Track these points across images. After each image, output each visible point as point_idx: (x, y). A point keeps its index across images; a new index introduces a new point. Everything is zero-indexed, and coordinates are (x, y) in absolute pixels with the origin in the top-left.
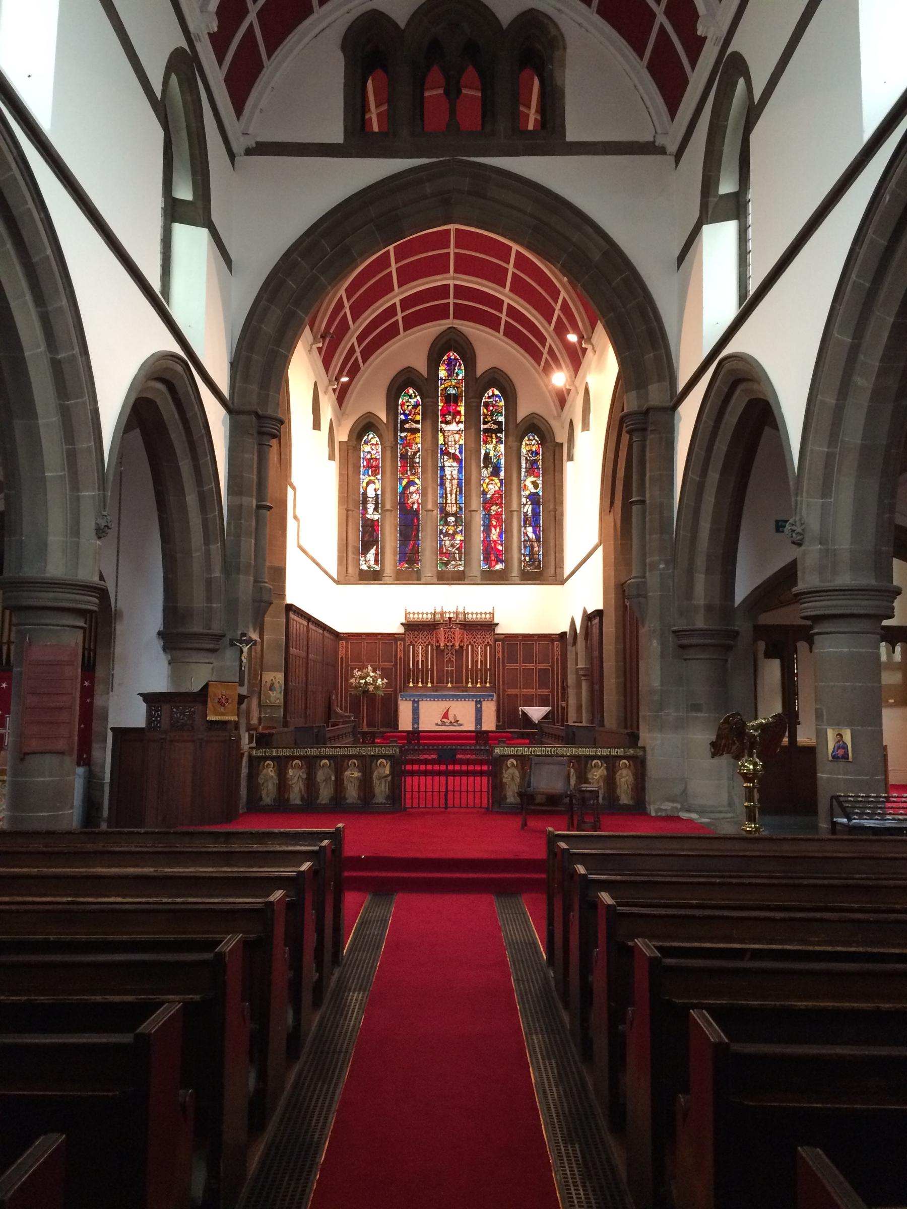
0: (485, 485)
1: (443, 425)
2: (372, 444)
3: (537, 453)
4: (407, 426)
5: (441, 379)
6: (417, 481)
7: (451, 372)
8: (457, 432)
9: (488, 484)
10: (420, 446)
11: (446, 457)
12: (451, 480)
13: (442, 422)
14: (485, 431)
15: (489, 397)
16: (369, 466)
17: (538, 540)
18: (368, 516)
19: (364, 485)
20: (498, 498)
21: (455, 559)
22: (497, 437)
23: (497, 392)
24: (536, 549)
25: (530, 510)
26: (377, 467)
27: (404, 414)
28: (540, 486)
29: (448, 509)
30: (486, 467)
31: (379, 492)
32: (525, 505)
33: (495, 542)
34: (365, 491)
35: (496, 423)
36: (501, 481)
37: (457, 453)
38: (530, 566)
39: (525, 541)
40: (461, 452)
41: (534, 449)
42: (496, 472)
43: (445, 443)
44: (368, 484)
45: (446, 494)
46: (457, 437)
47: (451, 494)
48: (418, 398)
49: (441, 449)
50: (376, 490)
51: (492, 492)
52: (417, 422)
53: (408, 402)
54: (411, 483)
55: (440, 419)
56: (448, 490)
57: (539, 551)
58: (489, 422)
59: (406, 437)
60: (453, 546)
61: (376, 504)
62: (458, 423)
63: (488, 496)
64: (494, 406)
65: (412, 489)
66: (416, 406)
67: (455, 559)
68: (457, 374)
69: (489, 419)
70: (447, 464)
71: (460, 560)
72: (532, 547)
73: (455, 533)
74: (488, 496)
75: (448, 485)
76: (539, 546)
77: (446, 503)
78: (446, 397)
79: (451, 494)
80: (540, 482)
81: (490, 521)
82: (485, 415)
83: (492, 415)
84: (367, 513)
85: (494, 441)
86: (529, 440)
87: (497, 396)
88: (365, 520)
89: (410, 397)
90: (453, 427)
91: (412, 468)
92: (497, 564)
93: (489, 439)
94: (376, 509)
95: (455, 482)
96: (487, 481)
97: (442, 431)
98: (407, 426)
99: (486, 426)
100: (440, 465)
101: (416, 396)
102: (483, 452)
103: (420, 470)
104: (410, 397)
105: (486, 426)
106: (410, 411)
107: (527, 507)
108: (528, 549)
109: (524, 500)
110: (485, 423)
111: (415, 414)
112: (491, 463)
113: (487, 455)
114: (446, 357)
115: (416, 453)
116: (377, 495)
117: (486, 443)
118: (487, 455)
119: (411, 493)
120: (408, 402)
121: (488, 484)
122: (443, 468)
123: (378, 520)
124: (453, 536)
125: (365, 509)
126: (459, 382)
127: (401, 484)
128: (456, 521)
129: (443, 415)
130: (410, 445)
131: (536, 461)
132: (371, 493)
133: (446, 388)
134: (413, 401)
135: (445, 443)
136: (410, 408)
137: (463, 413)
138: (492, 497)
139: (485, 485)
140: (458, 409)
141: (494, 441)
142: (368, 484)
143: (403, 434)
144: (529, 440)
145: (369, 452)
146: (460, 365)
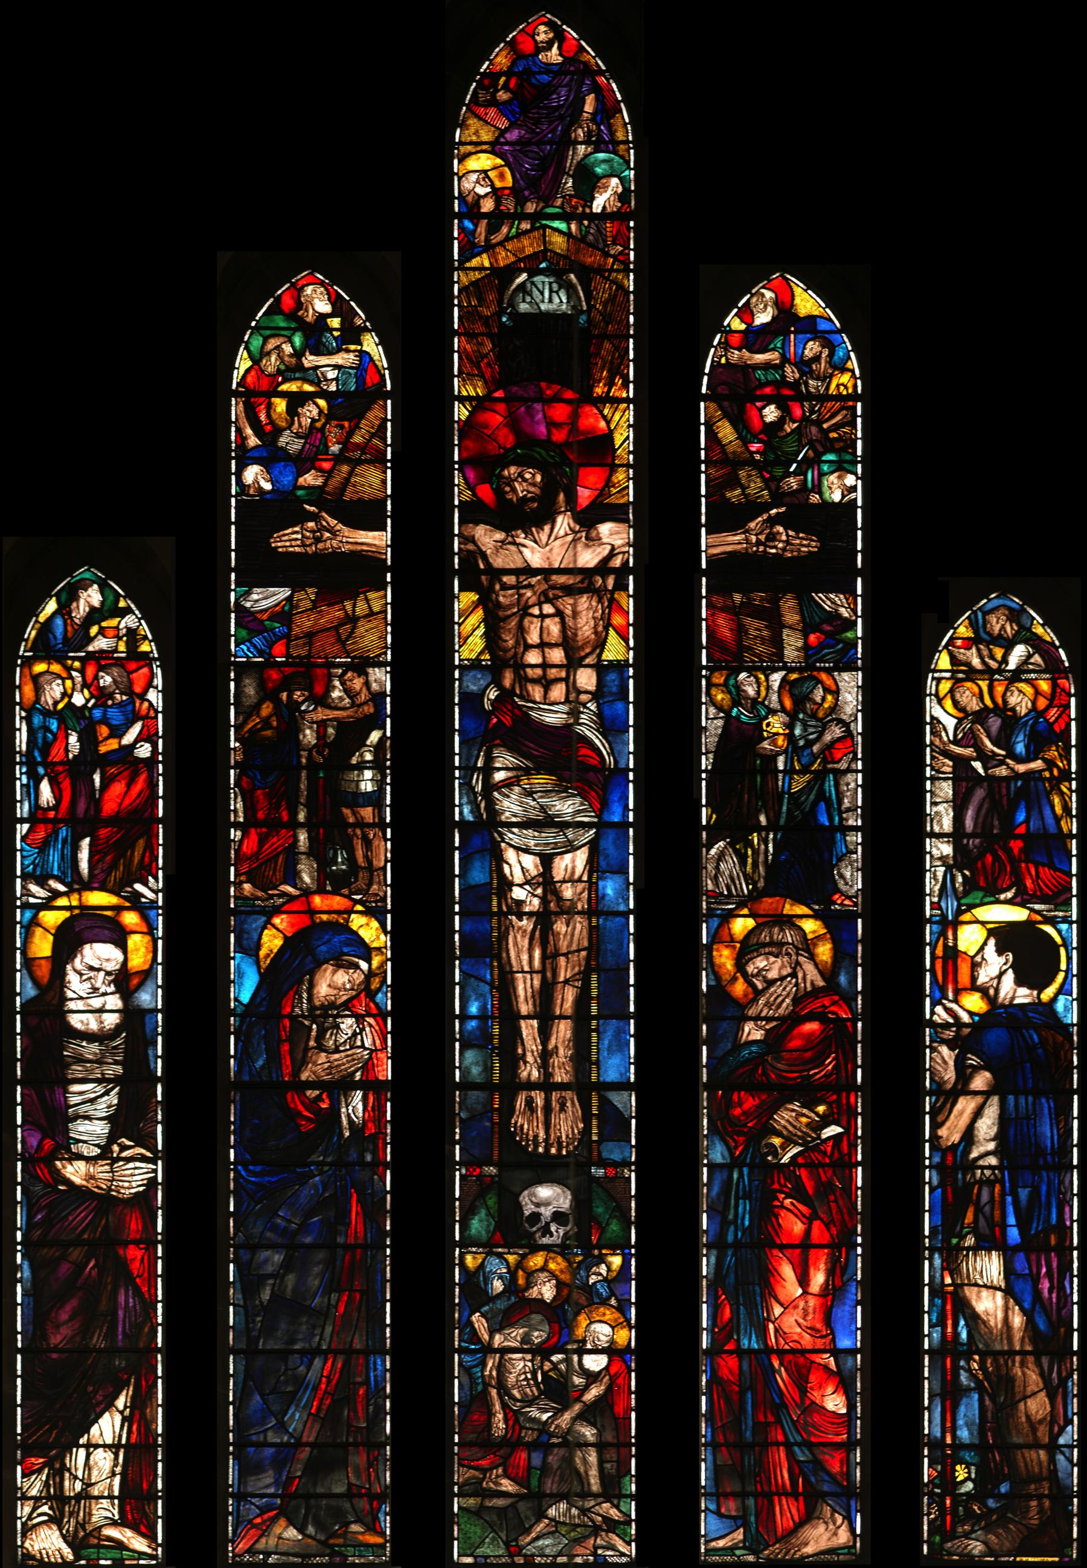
0: (725, 958)
1: (487, 537)
2: (103, 660)
3: (1043, 735)
4: (289, 540)
5: (472, 209)
6: (368, 929)
7: (540, 171)
8: (585, 581)
9: (747, 948)
10: (381, 678)
11: (504, 761)
12: (544, 919)
13: (473, 513)
14: (730, 571)
15: (756, 338)
16: (76, 817)
17: (1046, 1341)
18: (75, 1172)
19: (43, 946)
20: (818, 1048)
21: (574, 1489)
22: (814, 621)
23: (807, 303)
24: (1037, 1406)
25: (987, 1126)
26: (136, 821)
27: (270, 456)
28: (1069, 961)
29: (528, 1125)
30: (734, 829)
31: (150, 997)
32: (948, 1096)
33: (799, 1360)
34: (52, 989)
35: (804, 514)
36: (837, 925)
37: (587, 729)
38: (988, 1522)
39: (949, 1348)
40: (611, 727)
41: (1020, 700)
42: (802, 870)
43: (502, 658)
44: (69, 941)
45: (510, 1018)
46: (586, 613)
47: (546, 1017)
48: (370, 344)
49: (472, 701)
50: (125, 981)
51: (783, 1000)
52: (366, 515)
53: (294, 369)
54: (333, 943)
55: (460, 493)
56: (524, 988)
57: (1057, 1422)
58: (753, 508)
59: (284, 614)
60: (557, 1391)
61: (133, 1084)
62: (587, 521)
63: (753, 1032)
64: (786, 395)
65: (332, 983)
66: (349, 405)
67: (574, 1489)
68: (588, 182)
69: (755, 486)
70: (510, 806)
71: (611, 1491)
72: (1001, 1392)
73: (575, 1299)
74: (753, 1032)
75: (521, 951)
76: (1055, 1391)
77: (512, 1085)
78: (500, 337)
79: (546, 1017)
80: (1065, 933)
81: (766, 1212)
82: (730, 469)
83: (774, 463)
84: (65, 1148)
85: (792, 645)
86: (981, 638)
87: (809, 326)
88: (56, 1200)
89: (315, 335)
90: (547, 548)
91: (332, 832)
92: (808, 1517)
93: (755, 627)
94: (126, 1123)
95: (571, 932)
96: (741, 925)
97: (480, 576)
98: (289, 540)
99: (732, 541)
100: (463, 811)
101: (351, 335)
102: (711, 723)
103: (384, 850)
104: (315, 335)
105: (732, 541)
106: (314, 434)
107: (965, 1106)
108: (969, 1409)
109: (942, 1061)
110: (727, 518)
111: (355, 456)
112: (771, 799)
113: (741, 739)
114: (501, 58)
115: (352, 733)
116: (132, 1016)
117: (731, 658)
118: (741, 739)
119: (327, 1014)
120: (294, 369)
121: (747, 948)
122: (486, 836)
123: (143, 1200)
124: (561, 1316)
125: (54, 1123)
126: (596, 229)
127: (251, 949)
128: (581, 1214)
129: (486, 466)
130: (311, 675)
131: (1033, 791)
132: (91, 1002)
133: (502, 275)
134: (332, 366)
135: (502, 658)
136: (310, 412)
137: (624, 437)
138: (774, 1040)
139: (725, 958)
140: (593, 420)
141: (792, 645)
142: (69, 941)
143: (265, 599)
144: (981, 638)
145: (69, 715)
146: (606, 111)
